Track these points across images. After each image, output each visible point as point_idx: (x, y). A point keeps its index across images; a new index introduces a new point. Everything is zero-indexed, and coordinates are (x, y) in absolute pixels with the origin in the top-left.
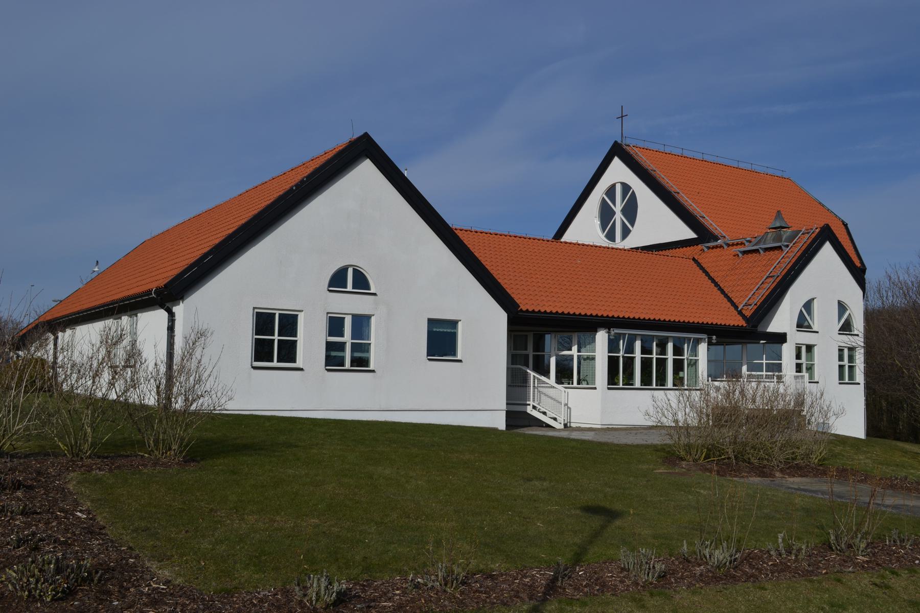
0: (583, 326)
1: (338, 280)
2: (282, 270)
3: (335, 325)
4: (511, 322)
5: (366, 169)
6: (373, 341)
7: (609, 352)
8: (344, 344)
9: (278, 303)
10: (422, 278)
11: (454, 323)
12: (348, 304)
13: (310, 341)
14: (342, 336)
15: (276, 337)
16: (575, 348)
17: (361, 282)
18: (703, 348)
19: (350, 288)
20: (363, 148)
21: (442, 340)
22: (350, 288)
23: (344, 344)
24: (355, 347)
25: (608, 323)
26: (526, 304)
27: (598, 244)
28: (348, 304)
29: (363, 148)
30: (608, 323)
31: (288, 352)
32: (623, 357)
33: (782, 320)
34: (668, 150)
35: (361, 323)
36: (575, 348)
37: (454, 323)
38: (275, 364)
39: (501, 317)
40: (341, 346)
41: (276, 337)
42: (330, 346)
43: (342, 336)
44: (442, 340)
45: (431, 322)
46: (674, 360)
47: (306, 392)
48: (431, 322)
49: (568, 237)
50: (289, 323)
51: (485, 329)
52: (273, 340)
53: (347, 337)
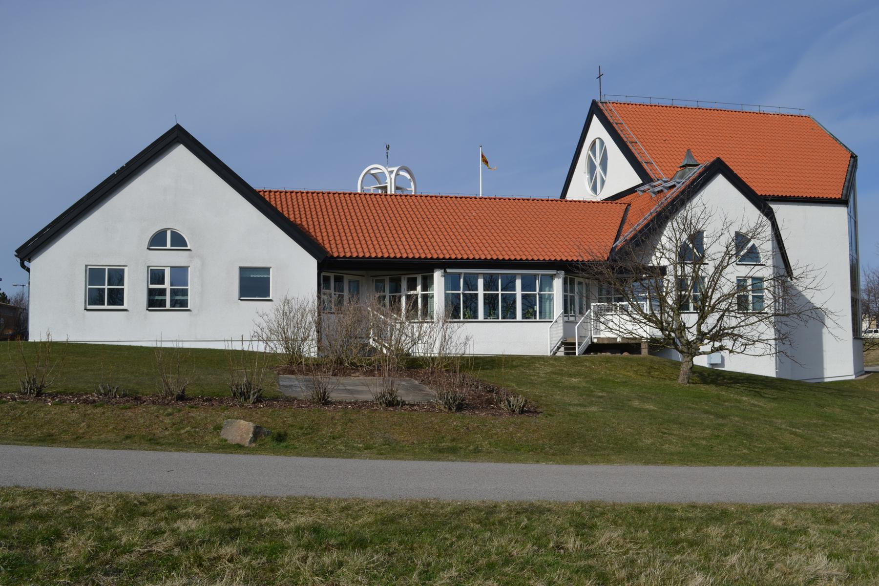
0: (421, 269)
1: (157, 240)
2: (114, 235)
3: (157, 276)
4: (321, 268)
5: (720, 182)
6: (126, 287)
7: (123, 289)
8: (165, 290)
9: (107, 261)
10: (231, 233)
11: (267, 270)
12: (165, 259)
13: (135, 289)
14: (163, 283)
15: (500, 292)
16: (419, 288)
17: (179, 241)
18: (558, 284)
19: (169, 246)
20: (178, 136)
21: (254, 284)
22: (169, 246)
23: (165, 290)
24: (174, 292)
25: (444, 264)
26: (337, 250)
27: (581, 199)
28: (165, 259)
29: (178, 136)
30: (444, 264)
31: (116, 298)
32: (464, 295)
33: (664, 253)
34: (654, 102)
35: (180, 273)
36: (419, 288)
37: (267, 270)
38: (106, 307)
39: (310, 264)
40: (162, 292)
41: (500, 292)
42: (151, 292)
43: (163, 283)
44: (254, 284)
45: (242, 269)
46: (485, 295)
47: (133, 327)
48: (242, 269)
49: (569, 197)
50: (117, 276)
51: (296, 275)
52: (105, 289)
53: (167, 285)
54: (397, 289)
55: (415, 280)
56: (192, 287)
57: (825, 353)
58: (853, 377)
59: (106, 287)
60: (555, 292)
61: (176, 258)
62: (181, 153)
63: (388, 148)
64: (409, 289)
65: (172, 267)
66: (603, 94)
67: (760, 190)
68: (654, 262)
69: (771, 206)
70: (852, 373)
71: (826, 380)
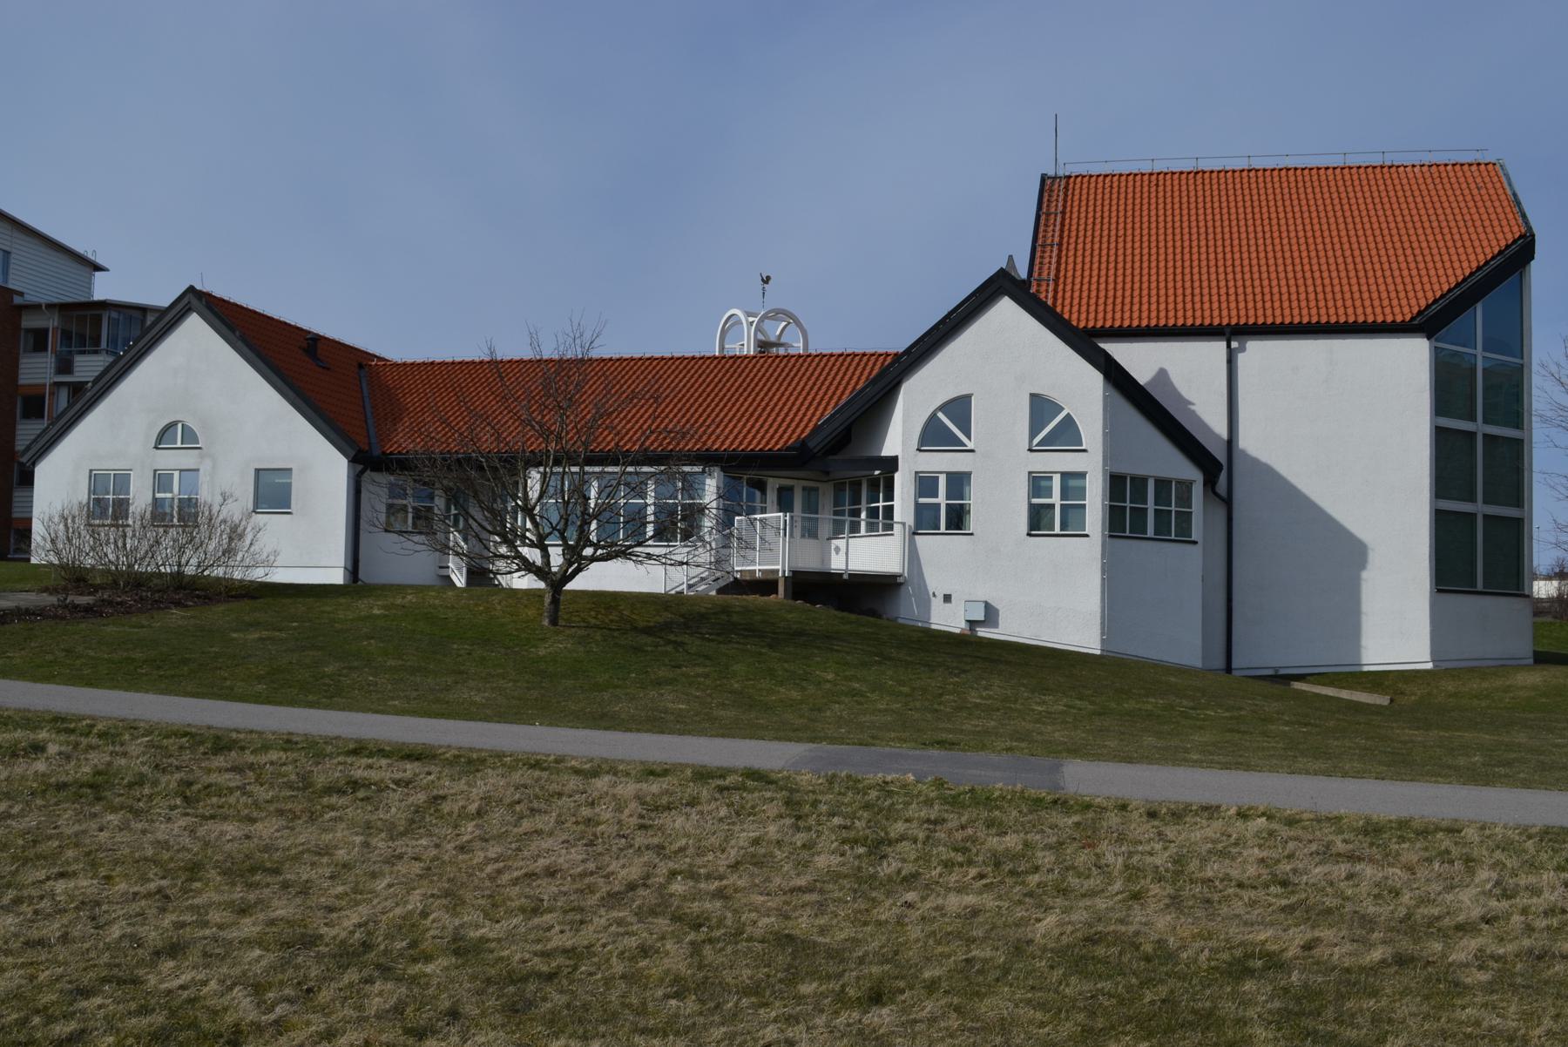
1: (164, 436)
3: (1038, 483)
5: (1006, 310)
15: (1128, 504)
17: (189, 436)
28: (171, 460)
35: (958, 482)
41: (1173, 508)
54: (856, 500)
55: (791, 489)
56: (976, 499)
57: (1364, 618)
58: (1430, 666)
59: (1128, 504)
60: (897, 503)
61: (186, 459)
62: (1006, 310)
63: (766, 280)
64: (870, 502)
65: (948, 474)
66: (1060, 161)
67: (1080, 320)
68: (887, 451)
69: (1102, 345)
70: (1428, 658)
71: (1366, 669)
